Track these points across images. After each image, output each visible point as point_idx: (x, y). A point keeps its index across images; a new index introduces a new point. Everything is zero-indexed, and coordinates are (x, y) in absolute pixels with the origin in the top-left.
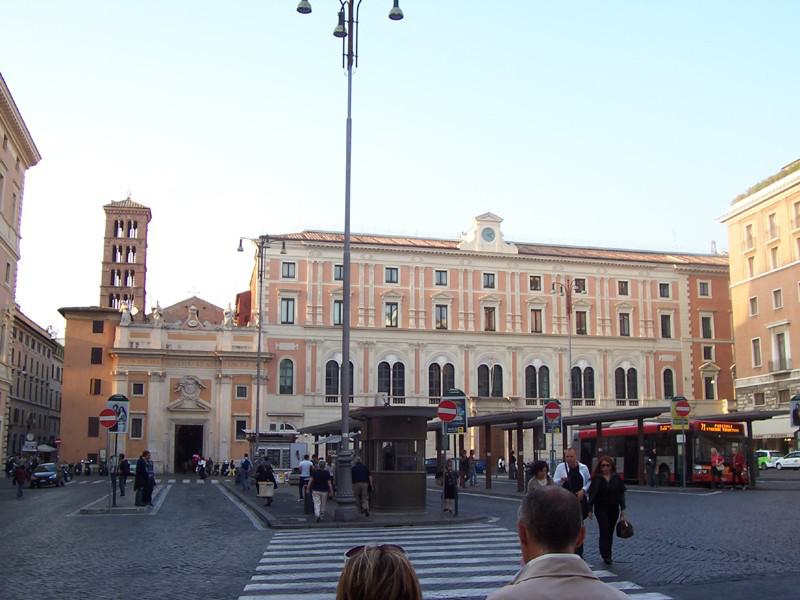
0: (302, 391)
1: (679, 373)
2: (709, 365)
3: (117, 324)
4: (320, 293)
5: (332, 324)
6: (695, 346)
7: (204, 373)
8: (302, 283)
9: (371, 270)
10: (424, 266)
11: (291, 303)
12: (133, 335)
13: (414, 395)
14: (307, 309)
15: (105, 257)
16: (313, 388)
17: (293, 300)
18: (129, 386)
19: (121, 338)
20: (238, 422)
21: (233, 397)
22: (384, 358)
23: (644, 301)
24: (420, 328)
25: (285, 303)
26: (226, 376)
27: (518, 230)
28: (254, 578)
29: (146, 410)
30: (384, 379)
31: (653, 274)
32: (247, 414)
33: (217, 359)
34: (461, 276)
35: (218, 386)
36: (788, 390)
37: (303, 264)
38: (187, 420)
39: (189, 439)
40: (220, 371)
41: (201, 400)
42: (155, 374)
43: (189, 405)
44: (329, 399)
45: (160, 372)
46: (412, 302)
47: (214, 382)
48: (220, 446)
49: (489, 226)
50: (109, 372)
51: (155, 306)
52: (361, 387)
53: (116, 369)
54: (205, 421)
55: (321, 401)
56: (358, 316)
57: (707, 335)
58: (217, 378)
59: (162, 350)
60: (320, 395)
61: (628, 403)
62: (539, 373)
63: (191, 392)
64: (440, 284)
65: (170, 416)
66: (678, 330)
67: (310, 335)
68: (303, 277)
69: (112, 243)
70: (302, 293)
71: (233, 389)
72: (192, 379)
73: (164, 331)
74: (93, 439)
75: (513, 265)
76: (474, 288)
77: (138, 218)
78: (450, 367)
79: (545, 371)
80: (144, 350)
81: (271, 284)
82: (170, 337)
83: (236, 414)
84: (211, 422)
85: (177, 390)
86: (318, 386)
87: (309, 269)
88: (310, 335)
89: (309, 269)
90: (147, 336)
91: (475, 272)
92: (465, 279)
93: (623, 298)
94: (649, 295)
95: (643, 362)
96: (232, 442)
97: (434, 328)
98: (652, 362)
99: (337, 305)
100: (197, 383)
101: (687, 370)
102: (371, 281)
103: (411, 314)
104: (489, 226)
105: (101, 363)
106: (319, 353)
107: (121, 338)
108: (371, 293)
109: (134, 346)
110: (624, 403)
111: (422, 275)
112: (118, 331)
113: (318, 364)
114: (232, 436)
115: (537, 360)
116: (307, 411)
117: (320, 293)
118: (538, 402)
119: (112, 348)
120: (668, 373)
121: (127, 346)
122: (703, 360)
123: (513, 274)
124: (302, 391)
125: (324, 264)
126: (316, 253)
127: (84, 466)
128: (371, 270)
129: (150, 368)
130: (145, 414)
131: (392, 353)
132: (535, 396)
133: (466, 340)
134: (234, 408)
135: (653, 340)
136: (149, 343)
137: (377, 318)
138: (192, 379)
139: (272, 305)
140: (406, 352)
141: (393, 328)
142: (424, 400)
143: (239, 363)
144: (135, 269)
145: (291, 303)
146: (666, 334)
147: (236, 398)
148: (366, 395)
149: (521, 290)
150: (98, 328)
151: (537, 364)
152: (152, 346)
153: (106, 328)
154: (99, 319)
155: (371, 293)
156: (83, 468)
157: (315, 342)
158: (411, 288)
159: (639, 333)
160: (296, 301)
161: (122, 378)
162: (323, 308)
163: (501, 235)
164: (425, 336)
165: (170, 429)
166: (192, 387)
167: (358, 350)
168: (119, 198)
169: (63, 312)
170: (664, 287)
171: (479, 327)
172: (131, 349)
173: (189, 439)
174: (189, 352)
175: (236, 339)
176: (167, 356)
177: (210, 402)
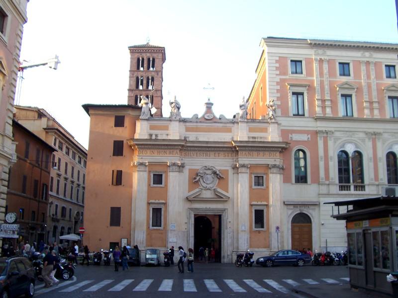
3: (137, 118)
4: (327, 87)
7: (221, 163)
8: (309, 78)
9: (372, 67)
10: (327, 58)
11: (300, 98)
12: (152, 128)
13: (373, 182)
14: (317, 102)
17: (302, 94)
19: (142, 130)
20: (256, 211)
21: (251, 187)
24: (375, 117)
26: (243, 166)
29: (166, 199)
30: (343, 167)
32: (265, 203)
33: (233, 149)
35: (235, 175)
37: (309, 62)
38: (206, 209)
39: (207, 229)
40: (238, 161)
41: (219, 190)
42: (174, 164)
43: (208, 195)
45: (179, 163)
46: (365, 90)
47: (231, 172)
48: (237, 237)
50: (130, 164)
51: (173, 101)
52: (372, 176)
53: (136, 159)
54: (225, 210)
55: (335, 189)
56: (364, 108)
58: (235, 168)
59: (180, 140)
60: (333, 184)
63: (210, 181)
64: (389, 77)
65: (189, 205)
67: (322, 126)
68: (310, 73)
70: (310, 87)
71: (250, 177)
72: (209, 169)
74: (115, 228)
76: (323, 80)
78: (359, 155)
80: (164, 140)
81: (280, 79)
82: (188, 130)
83: (151, 201)
84: (230, 211)
85: (195, 179)
87: (315, 66)
88: (322, 126)
89: (315, 66)
91: (329, 61)
92: (321, 69)
93: (344, 79)
96: (251, 231)
99: (294, 97)
100: (215, 173)
102: (373, 76)
103: (365, 104)
105: (122, 155)
106: (330, 143)
107: (142, 130)
108: (374, 87)
109: (154, 137)
110: (348, 188)
112: (139, 125)
114: (251, 225)
117: (327, 87)
118: (352, 188)
119: (133, 139)
121: (146, 137)
124: (316, 181)
126: (320, 51)
127: (103, 255)
128: (372, 67)
129: (170, 158)
130: (267, 205)
132: (349, 182)
134: (150, 195)
136: (168, 135)
137: (382, 109)
139: (283, 98)
141: (348, 118)
143: (255, 153)
145: (300, 98)
147: (254, 187)
148: (377, 183)
150: (119, 122)
151: (350, 149)
152: (170, 137)
153: (127, 122)
154: (121, 113)
155: (374, 87)
156: (103, 258)
157: (327, 132)
158: (315, 79)
161: (142, 168)
162: (331, 101)
165: (189, 218)
166: (210, 177)
167: (367, 140)
169: (87, 108)
170: (296, 62)
172: (151, 140)
173: (207, 229)
174: (207, 142)
177: (228, 192)
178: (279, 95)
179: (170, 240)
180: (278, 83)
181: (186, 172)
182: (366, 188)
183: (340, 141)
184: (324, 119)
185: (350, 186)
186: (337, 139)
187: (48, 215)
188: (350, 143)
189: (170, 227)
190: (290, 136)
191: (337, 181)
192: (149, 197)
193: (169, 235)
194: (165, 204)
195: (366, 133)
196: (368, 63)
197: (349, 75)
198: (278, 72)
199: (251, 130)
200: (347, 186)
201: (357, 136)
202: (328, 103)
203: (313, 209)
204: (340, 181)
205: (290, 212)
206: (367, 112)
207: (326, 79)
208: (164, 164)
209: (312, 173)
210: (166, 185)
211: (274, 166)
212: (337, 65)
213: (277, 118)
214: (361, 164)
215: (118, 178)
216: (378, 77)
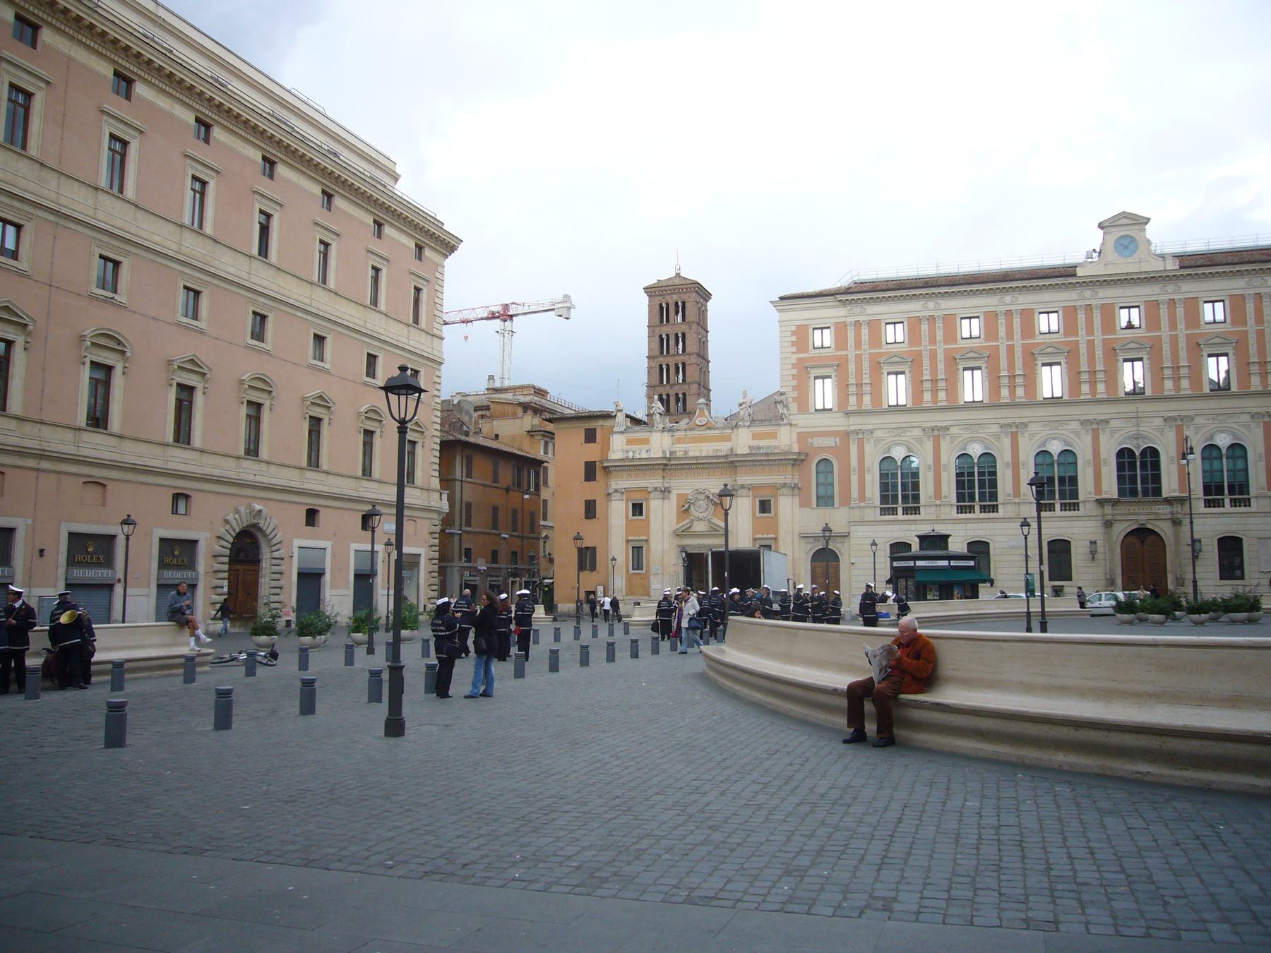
0: (846, 501)
10: (1018, 307)
15: (650, 350)
16: (862, 497)
18: (754, 507)
21: (754, 515)
26: (743, 487)
27: (1176, 229)
28: (183, 660)
29: (648, 535)
34: (1081, 317)
38: (699, 546)
43: (699, 527)
44: (884, 511)
55: (874, 514)
65: (677, 542)
69: (657, 332)
73: (666, 434)
75: (1171, 287)
77: (685, 297)
79: (1238, 452)
85: (685, 509)
86: (945, 492)
88: (856, 423)
90: (646, 441)
97: (1208, 391)
111: (1017, 321)
116: (853, 528)
123: (858, 324)
124: (846, 501)
125: (869, 323)
131: (974, 440)
132: (1223, 494)
133: (1094, 412)
144: (686, 359)
151: (1055, 448)
159: (1079, 393)
163: (1149, 242)
166: (703, 503)
167: (925, 439)
168: (666, 274)
174: (696, 458)
175: (755, 437)
176: (667, 466)
178: (795, 383)
179: (653, 587)
180: (794, 366)
181: (673, 497)
182: (922, 509)
183: (1204, 430)
184: (860, 413)
186: (878, 441)
187: (541, 554)
188: (1221, 432)
189: (653, 569)
192: (628, 534)
193: (652, 579)
194: (647, 541)
196: (932, 319)
198: (794, 349)
199: (755, 437)
202: (867, 389)
204: (960, 497)
205: (809, 546)
208: (645, 490)
209: (840, 492)
210: (776, 514)
211: (785, 485)
214: (1156, 465)
215: (590, 509)
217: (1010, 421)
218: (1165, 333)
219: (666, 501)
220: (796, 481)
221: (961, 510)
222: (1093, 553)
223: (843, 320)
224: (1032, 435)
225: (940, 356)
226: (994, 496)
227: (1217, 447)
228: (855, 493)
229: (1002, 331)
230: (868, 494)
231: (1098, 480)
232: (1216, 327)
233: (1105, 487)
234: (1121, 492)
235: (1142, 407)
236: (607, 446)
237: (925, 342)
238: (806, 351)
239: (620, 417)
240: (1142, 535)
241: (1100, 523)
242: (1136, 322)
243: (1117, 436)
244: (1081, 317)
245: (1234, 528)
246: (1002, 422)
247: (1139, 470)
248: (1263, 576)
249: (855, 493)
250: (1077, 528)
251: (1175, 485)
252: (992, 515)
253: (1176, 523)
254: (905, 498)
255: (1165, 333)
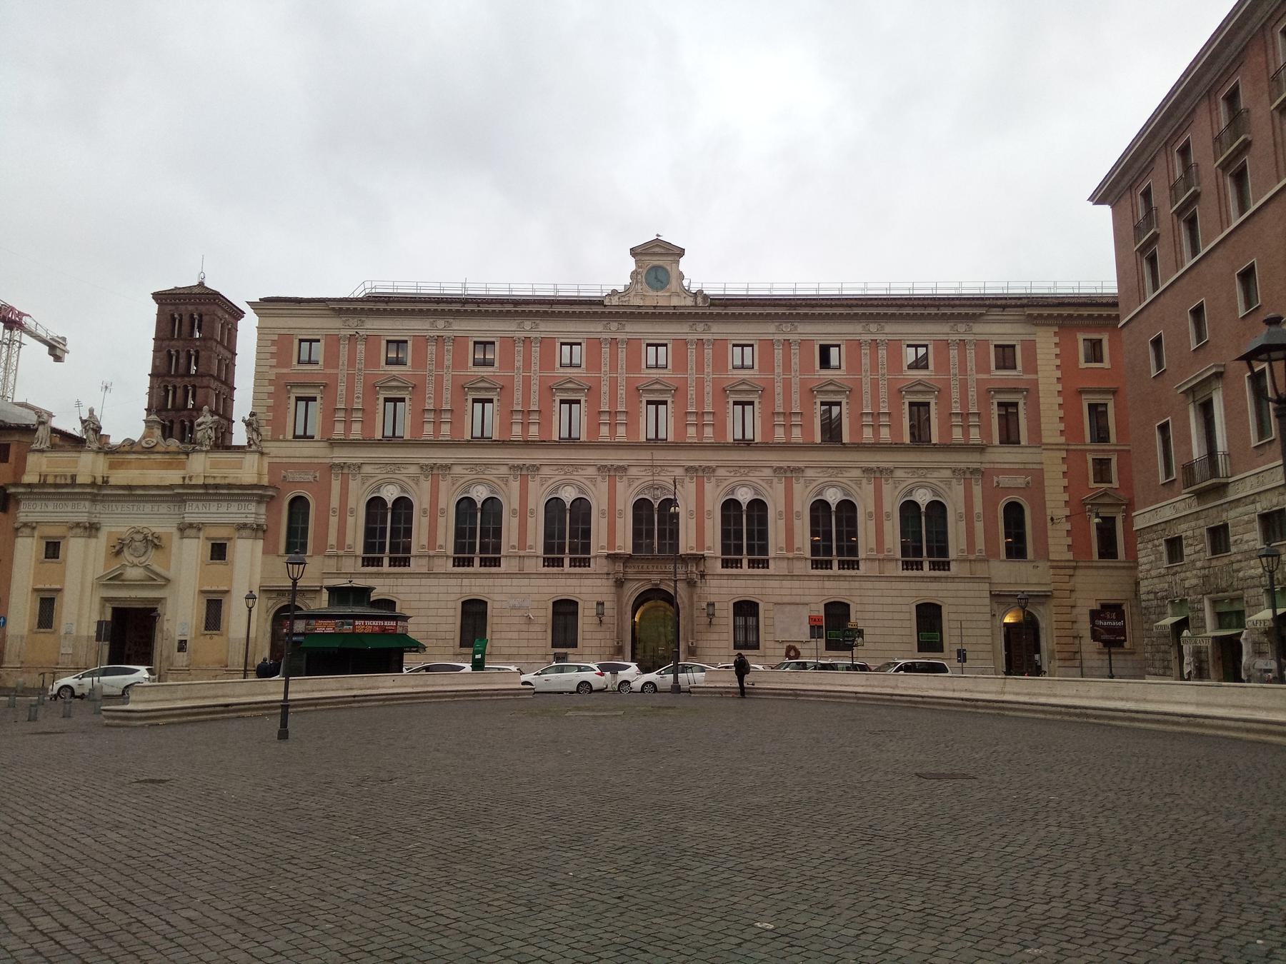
1: (1040, 506)
2: (1105, 494)
5: (378, 436)
6: (1072, 457)
7: (159, 520)
9: (795, 350)
12: (214, 466)
22: (820, 493)
23: (967, 379)
25: (565, 407)
31: (978, 328)
34: (778, 353)
36: (1225, 526)
38: (125, 600)
47: (176, 534)
49: (657, 258)
52: (873, 544)
54: (159, 600)
55: (805, 568)
57: (1100, 434)
61: (926, 565)
62: (482, 509)
66: (1036, 430)
72: (138, 532)
73: (101, 456)
82: (112, 466)
84: (169, 603)
86: (798, 542)
91: (977, 344)
94: (971, 364)
95: (959, 489)
98: (977, 491)
100: (145, 538)
101: (1056, 500)
102: (535, 367)
104: (657, 258)
106: (353, 485)
108: (622, 382)
110: (560, 563)
113: (531, 505)
115: (832, 490)
120: (1014, 513)
122: (1092, 485)
124: (320, 550)
133: (613, 458)
135: (981, 449)
138: (138, 532)
140: (947, 482)
141: (392, 441)
142: (891, 565)
146: (1009, 437)
148: (881, 556)
149: (629, 369)
160: (756, 404)
163: (681, 276)
164: (709, 455)
167: (775, 480)
171: (373, 428)
182: (861, 564)
183: (815, 484)
185: (831, 562)
186: (367, 477)
190: (995, 479)
191: (808, 555)
195: (601, 469)
196: (875, 344)
197: (1015, 368)
198: (274, 362)
200: (495, 559)
201: (404, 471)
203: (311, 599)
204: (905, 552)
205: (271, 603)
206: (604, 430)
207: (622, 375)
212: (992, 348)
213: (263, 444)
214: (763, 521)
216: (982, 367)
217: (521, 462)
218: (692, 375)
219: (94, 540)
220: (262, 520)
221: (458, 562)
222: (600, 615)
223: (336, 332)
224: (544, 481)
225: (447, 383)
226: (764, 549)
227: (827, 504)
228: (332, 539)
229: (519, 362)
230: (349, 540)
231: (612, 532)
232: (655, 374)
233: (619, 542)
234: (636, 547)
235: (660, 455)
236: (20, 468)
237: (778, 370)
238: (288, 365)
239: (42, 432)
240: (652, 595)
241: (611, 582)
242: (576, 361)
243: (635, 484)
244: (778, 353)
245: (570, 590)
246: (511, 462)
247: (656, 521)
248: (778, 645)
249: (332, 539)
250: (588, 588)
251: (693, 543)
252: (493, 570)
253: (691, 584)
254: (484, 548)
255: (692, 375)
